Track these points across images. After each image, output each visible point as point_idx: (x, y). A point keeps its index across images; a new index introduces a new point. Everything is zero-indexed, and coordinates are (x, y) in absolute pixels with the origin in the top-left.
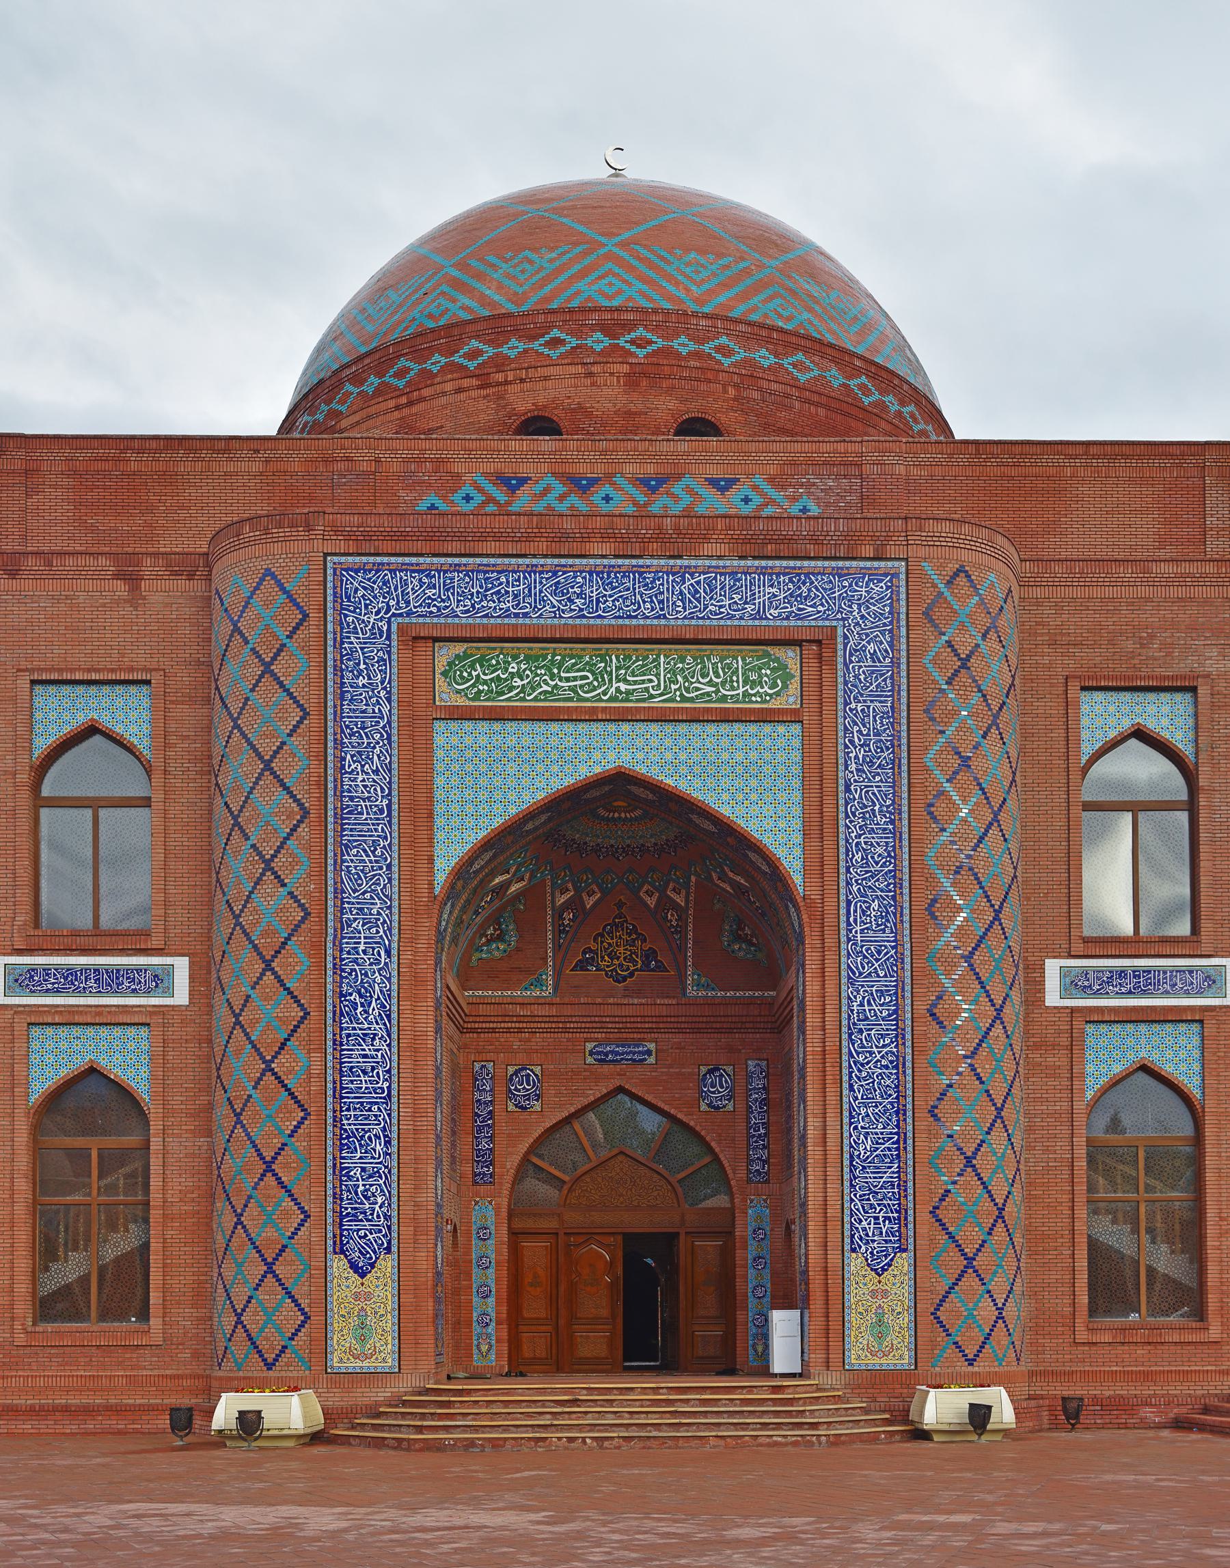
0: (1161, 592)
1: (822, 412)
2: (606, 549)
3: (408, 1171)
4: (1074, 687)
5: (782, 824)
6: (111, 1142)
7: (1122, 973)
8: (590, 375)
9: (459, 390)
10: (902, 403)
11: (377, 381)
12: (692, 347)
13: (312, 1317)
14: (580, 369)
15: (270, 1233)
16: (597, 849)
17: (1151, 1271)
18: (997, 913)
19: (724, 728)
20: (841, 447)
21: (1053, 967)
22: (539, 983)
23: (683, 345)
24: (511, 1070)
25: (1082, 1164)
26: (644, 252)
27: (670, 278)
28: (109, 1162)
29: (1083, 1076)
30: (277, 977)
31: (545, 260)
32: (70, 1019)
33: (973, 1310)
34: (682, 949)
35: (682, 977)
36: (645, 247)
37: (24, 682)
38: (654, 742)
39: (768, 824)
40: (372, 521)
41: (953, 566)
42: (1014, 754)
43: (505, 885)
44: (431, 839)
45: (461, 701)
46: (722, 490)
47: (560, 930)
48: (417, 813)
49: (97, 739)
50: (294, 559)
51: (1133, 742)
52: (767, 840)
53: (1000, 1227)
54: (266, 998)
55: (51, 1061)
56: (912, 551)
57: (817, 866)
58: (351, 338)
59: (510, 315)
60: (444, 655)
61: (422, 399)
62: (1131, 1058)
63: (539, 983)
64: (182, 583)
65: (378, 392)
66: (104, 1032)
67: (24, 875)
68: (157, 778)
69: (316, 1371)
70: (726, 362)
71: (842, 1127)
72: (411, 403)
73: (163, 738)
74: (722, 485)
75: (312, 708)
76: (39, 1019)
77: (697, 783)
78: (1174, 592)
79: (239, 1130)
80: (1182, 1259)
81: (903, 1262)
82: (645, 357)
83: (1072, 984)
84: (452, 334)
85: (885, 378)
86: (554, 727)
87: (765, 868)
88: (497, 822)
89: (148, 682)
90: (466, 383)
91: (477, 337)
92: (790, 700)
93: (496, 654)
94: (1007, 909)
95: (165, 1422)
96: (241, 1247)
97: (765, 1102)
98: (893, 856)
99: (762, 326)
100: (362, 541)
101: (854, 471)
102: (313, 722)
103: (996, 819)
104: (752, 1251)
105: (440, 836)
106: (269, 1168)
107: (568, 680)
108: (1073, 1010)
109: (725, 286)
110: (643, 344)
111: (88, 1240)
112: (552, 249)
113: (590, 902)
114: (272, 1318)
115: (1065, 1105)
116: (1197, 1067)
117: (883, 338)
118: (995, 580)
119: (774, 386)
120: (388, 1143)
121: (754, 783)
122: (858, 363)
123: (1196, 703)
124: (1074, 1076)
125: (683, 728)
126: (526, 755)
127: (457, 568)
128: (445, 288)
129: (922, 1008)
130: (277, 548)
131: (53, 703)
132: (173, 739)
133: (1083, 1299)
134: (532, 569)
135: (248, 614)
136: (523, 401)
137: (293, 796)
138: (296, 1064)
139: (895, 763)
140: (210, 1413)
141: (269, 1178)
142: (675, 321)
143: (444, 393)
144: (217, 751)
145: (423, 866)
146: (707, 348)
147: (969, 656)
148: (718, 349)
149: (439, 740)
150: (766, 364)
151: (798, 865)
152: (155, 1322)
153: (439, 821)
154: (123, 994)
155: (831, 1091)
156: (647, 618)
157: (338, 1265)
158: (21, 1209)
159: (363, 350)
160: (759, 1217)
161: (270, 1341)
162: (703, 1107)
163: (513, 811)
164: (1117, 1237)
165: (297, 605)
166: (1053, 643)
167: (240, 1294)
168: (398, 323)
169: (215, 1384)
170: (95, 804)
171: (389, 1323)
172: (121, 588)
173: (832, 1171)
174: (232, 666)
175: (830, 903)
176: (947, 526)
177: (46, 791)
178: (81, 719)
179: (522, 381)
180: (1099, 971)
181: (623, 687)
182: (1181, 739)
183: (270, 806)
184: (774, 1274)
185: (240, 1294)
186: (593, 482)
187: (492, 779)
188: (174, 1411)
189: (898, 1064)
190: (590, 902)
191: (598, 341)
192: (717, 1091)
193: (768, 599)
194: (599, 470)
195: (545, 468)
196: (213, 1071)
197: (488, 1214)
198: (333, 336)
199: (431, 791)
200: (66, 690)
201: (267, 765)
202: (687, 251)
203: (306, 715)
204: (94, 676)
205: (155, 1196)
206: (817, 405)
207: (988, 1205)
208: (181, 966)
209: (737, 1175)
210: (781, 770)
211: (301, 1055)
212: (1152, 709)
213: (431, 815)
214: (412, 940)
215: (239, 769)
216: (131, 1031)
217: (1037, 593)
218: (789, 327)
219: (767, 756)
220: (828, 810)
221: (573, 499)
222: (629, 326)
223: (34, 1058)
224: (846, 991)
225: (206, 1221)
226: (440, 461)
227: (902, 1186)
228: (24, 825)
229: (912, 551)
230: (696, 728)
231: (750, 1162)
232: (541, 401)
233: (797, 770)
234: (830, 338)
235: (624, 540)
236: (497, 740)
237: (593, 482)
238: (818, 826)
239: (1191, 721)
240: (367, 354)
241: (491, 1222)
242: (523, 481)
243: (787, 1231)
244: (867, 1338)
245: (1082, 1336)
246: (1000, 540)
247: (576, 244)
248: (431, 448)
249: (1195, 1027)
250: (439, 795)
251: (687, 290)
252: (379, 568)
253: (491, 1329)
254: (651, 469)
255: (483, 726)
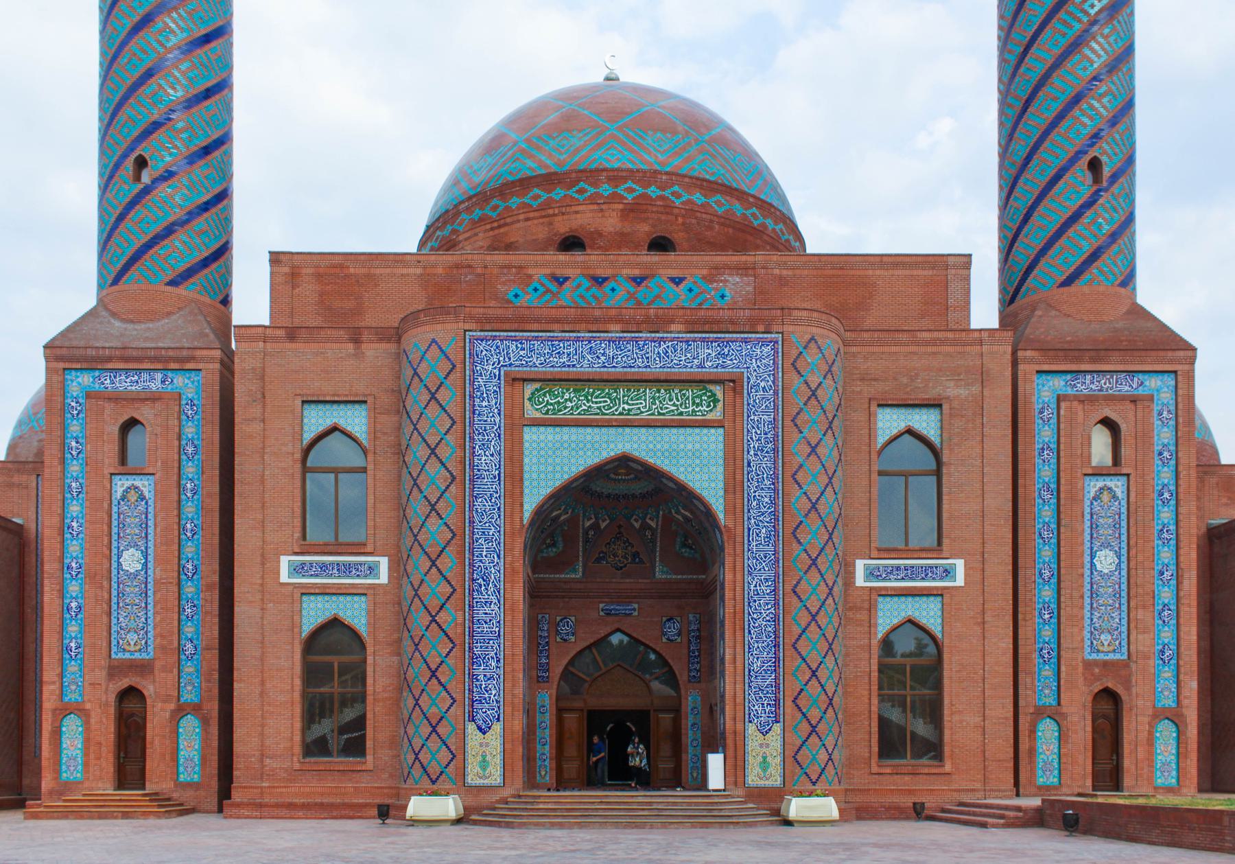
0: (923, 349)
1: (731, 231)
2: (618, 327)
3: (509, 677)
4: (874, 407)
5: (713, 485)
6: (345, 659)
7: (898, 568)
8: (602, 210)
9: (527, 219)
10: (776, 223)
11: (480, 212)
12: (659, 192)
13: (457, 756)
14: (595, 207)
15: (434, 710)
16: (608, 496)
17: (913, 734)
18: (831, 534)
19: (682, 430)
20: (744, 258)
21: (860, 565)
22: (575, 571)
23: (653, 191)
24: (558, 619)
25: (875, 674)
26: (632, 133)
27: (644, 148)
28: (344, 669)
29: (876, 625)
30: (439, 570)
31: (576, 140)
32: (325, 591)
33: (815, 755)
34: (654, 551)
35: (653, 567)
36: (633, 130)
37: (298, 402)
38: (643, 438)
39: (705, 485)
40: (490, 311)
41: (808, 337)
42: (840, 444)
43: (558, 517)
44: (522, 493)
45: (538, 415)
46: (677, 284)
47: (586, 541)
48: (514, 476)
49: (337, 433)
50: (446, 333)
51: (907, 435)
52: (704, 494)
53: (830, 710)
54: (433, 581)
55: (314, 613)
56: (786, 328)
57: (731, 509)
58: (465, 185)
59: (556, 173)
60: (529, 389)
61: (506, 225)
62: (903, 616)
63: (575, 571)
64: (384, 346)
65: (481, 219)
66: (342, 598)
67: (298, 511)
68: (371, 457)
69: (461, 785)
70: (678, 202)
71: (747, 655)
72: (499, 227)
73: (374, 433)
74: (677, 281)
75: (458, 419)
76: (307, 591)
77: (667, 462)
78: (930, 349)
79: (417, 654)
80: (931, 727)
81: (777, 728)
82: (634, 199)
83: (871, 574)
84: (525, 184)
85: (766, 207)
86: (589, 430)
87: (702, 508)
88: (558, 484)
89: (365, 402)
90: (531, 215)
91: (537, 186)
92: (717, 414)
93: (557, 390)
94: (836, 533)
95: (375, 812)
96: (417, 717)
97: (698, 637)
98: (774, 502)
99: (697, 179)
100: (485, 323)
101: (750, 272)
102: (457, 427)
103: (830, 482)
104: (691, 720)
105: (526, 491)
106: (434, 674)
107: (597, 403)
108: (871, 589)
109: (676, 154)
110: (630, 192)
111: (332, 711)
112: (580, 131)
113: (603, 525)
114: (435, 756)
115: (867, 641)
116: (939, 621)
117: (766, 183)
118: (830, 343)
119: (704, 216)
120: (498, 661)
121: (698, 461)
122: (751, 200)
123: (941, 414)
124: (871, 625)
125: (658, 431)
126: (573, 445)
127: (536, 338)
128: (518, 155)
129: (789, 588)
130: (439, 327)
131: (313, 413)
132: (379, 435)
133: (875, 749)
134: (578, 339)
135: (423, 365)
136: (563, 226)
137: (447, 469)
138: (448, 618)
139: (775, 450)
140: (405, 807)
141: (434, 681)
142: (648, 177)
143: (518, 221)
144: (404, 443)
145: (517, 507)
146: (667, 193)
147: (809, 455)
148: (673, 194)
149: (526, 437)
150: (699, 202)
151: (721, 508)
152: (369, 758)
153: (526, 483)
154: (352, 577)
155: (738, 633)
156: (639, 368)
157: (471, 728)
158: (297, 696)
159: (472, 193)
160: (695, 702)
161: (434, 769)
162: (664, 640)
163: (566, 477)
164: (895, 715)
165: (449, 360)
166: (862, 380)
167: (417, 743)
168: (492, 177)
169: (403, 792)
170: (336, 471)
171: (498, 760)
172: (351, 346)
173: (739, 678)
174: (412, 392)
175: (739, 529)
176: (805, 313)
177: (309, 464)
178: (328, 423)
179: (563, 214)
180: (886, 566)
181: (626, 407)
182: (932, 434)
183: (435, 476)
184: (703, 733)
185: (417, 743)
186: (605, 279)
187: (555, 459)
188: (380, 806)
189: (776, 619)
190: (603, 525)
191: (606, 189)
192: (672, 630)
193: (703, 356)
194: (608, 272)
195: (579, 271)
196: (404, 621)
197: (546, 698)
198: (493, 144)
199: (522, 466)
200: (320, 406)
201: (433, 452)
202: (655, 131)
203: (454, 423)
204: (336, 399)
205: (370, 689)
206: (729, 226)
207: (824, 697)
208: (384, 562)
209: (682, 677)
210: (713, 454)
211: (451, 612)
212: (917, 417)
213: (522, 480)
214: (512, 550)
215: (419, 452)
216: (356, 598)
217: (854, 349)
218: (712, 179)
219: (705, 446)
220: (738, 477)
221: (594, 290)
222: (625, 180)
223: (304, 612)
224: (748, 578)
225: (397, 702)
226: (521, 267)
227: (777, 686)
228: (298, 483)
229: (786, 328)
230: (666, 431)
231: (690, 671)
232: (1194, 531)
233: (721, 454)
234: (735, 185)
235: (479, 321)
236: (558, 437)
237: (605, 279)
238: (733, 486)
239: (939, 424)
240: (476, 195)
241: (547, 703)
242: (567, 279)
243: (712, 709)
244: (758, 770)
245: (875, 769)
246: (834, 320)
247: (593, 128)
248: (514, 258)
249: (939, 599)
250: (526, 468)
251: (657, 157)
252: (494, 338)
253: (547, 763)
254: (637, 272)
255: (550, 430)
